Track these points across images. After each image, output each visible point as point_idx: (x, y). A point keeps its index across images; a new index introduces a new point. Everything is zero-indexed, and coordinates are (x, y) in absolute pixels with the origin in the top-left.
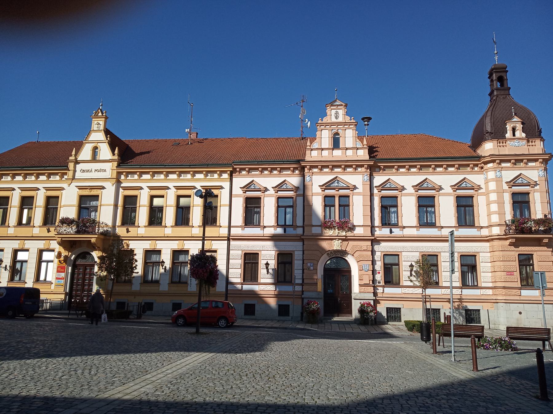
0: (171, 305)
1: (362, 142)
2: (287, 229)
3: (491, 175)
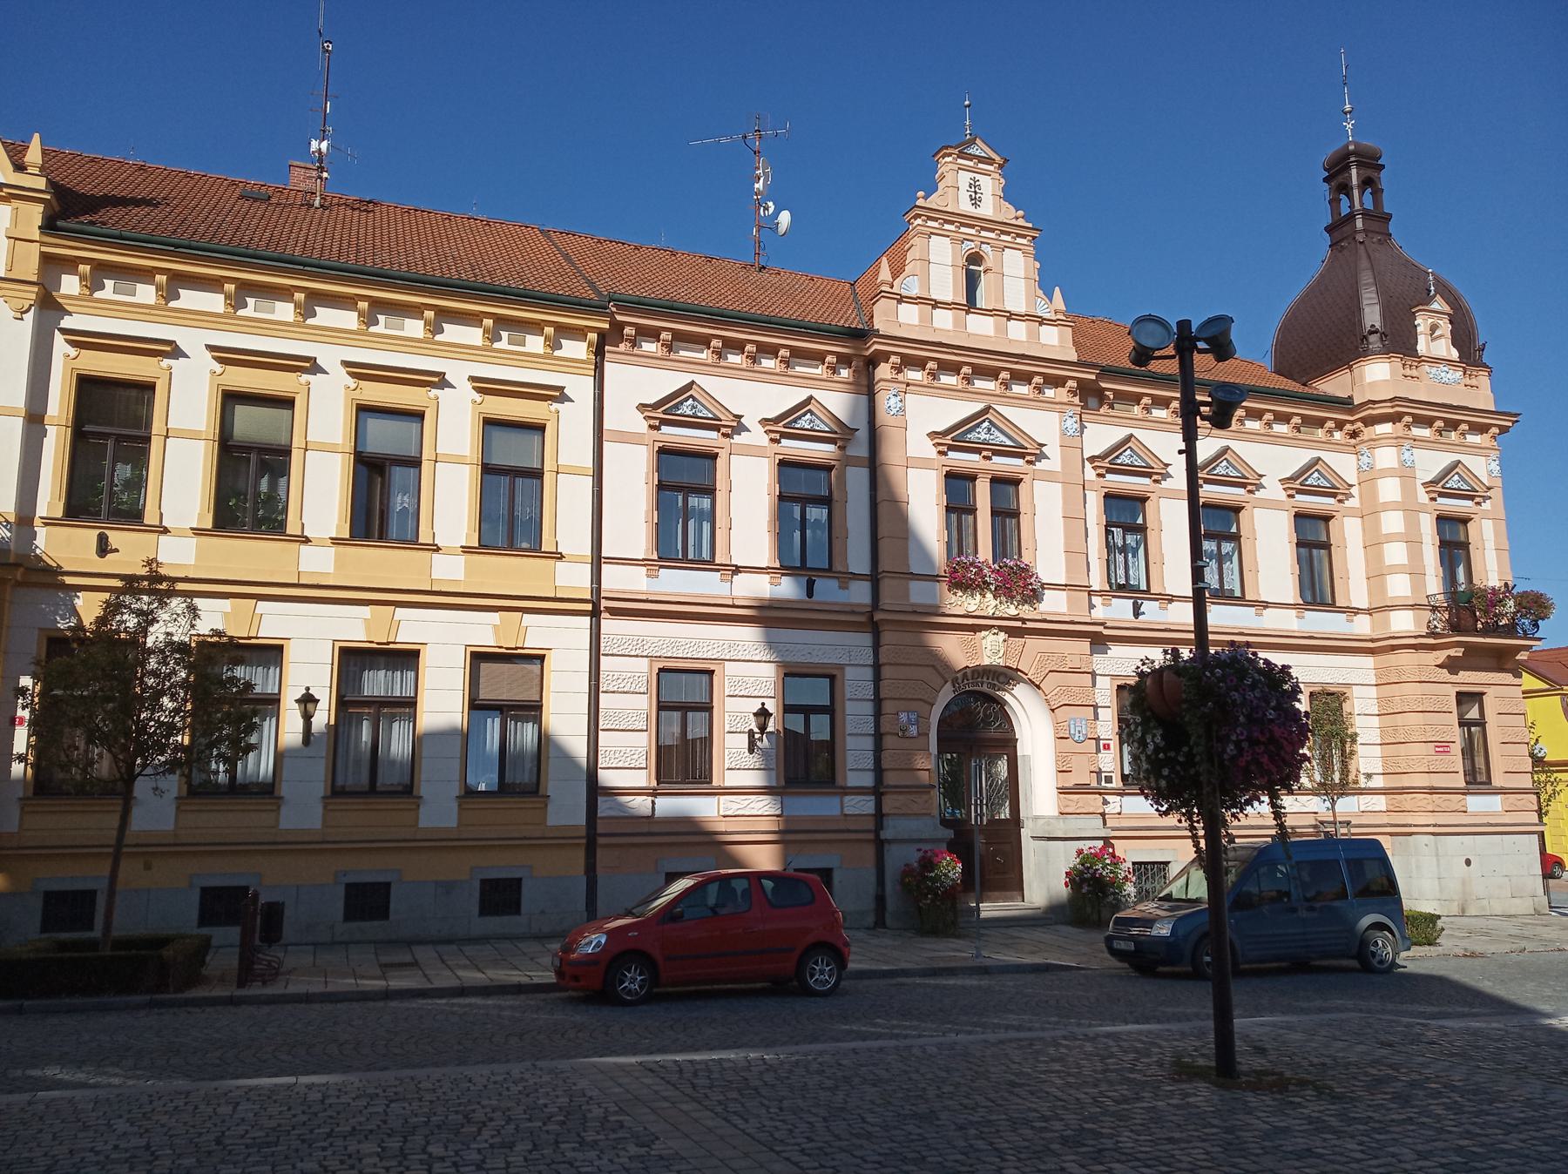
0: (195, 897)
2: (820, 584)
3: (1386, 457)
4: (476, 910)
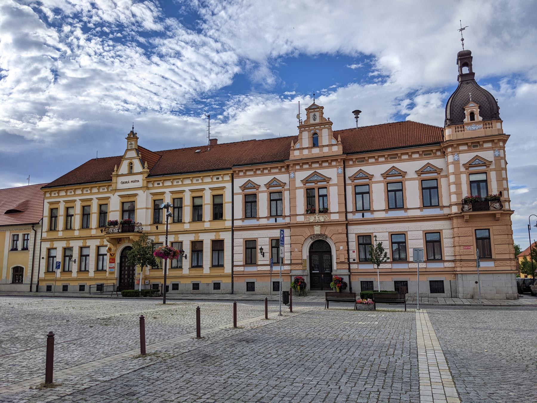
0: (192, 285)
1: (337, 139)
2: (365, 214)
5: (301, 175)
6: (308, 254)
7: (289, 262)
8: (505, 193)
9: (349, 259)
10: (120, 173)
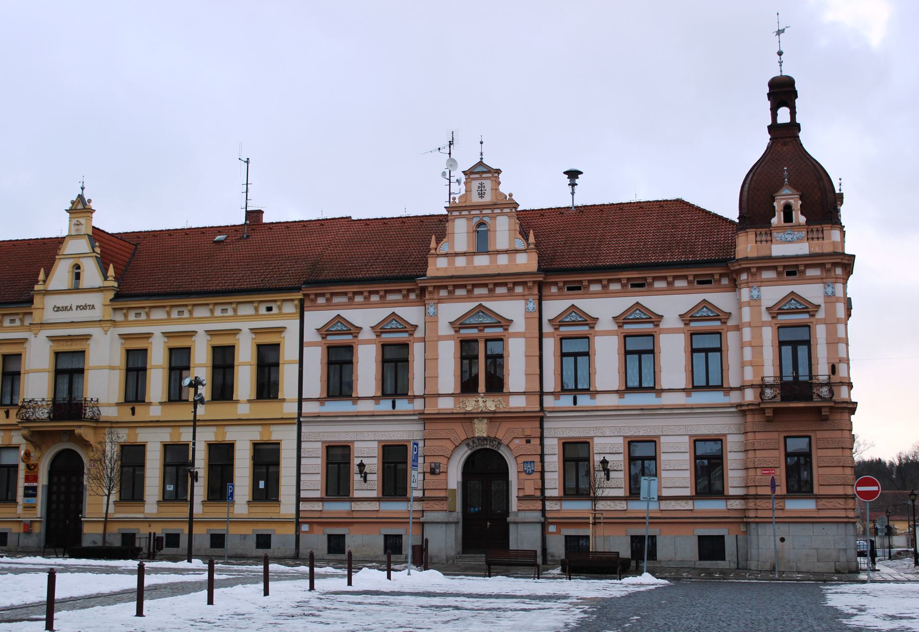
0: (209, 536)
1: (527, 239)
2: (398, 402)
4: (254, 546)
5: (451, 311)
6: (460, 479)
7: (419, 494)
8: (842, 368)
9: (543, 490)
10: (53, 284)
